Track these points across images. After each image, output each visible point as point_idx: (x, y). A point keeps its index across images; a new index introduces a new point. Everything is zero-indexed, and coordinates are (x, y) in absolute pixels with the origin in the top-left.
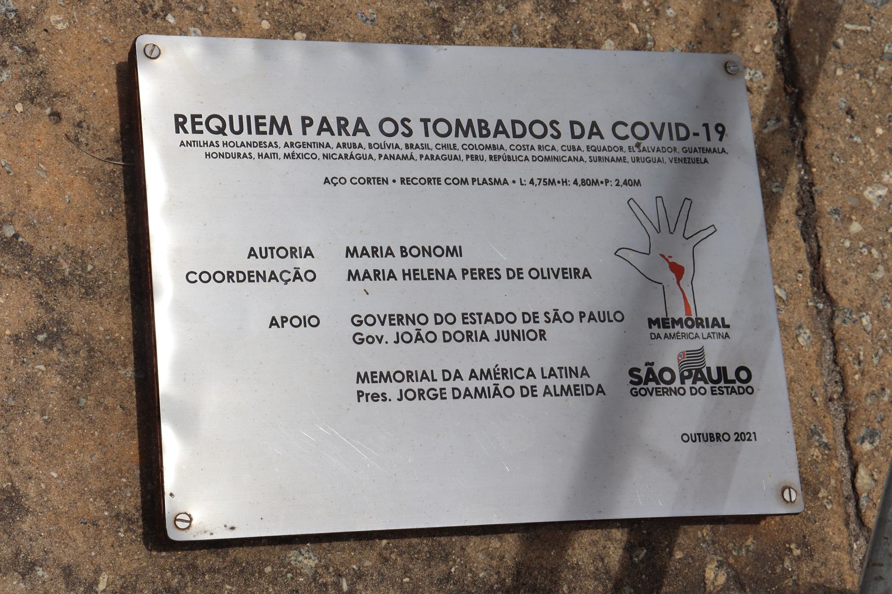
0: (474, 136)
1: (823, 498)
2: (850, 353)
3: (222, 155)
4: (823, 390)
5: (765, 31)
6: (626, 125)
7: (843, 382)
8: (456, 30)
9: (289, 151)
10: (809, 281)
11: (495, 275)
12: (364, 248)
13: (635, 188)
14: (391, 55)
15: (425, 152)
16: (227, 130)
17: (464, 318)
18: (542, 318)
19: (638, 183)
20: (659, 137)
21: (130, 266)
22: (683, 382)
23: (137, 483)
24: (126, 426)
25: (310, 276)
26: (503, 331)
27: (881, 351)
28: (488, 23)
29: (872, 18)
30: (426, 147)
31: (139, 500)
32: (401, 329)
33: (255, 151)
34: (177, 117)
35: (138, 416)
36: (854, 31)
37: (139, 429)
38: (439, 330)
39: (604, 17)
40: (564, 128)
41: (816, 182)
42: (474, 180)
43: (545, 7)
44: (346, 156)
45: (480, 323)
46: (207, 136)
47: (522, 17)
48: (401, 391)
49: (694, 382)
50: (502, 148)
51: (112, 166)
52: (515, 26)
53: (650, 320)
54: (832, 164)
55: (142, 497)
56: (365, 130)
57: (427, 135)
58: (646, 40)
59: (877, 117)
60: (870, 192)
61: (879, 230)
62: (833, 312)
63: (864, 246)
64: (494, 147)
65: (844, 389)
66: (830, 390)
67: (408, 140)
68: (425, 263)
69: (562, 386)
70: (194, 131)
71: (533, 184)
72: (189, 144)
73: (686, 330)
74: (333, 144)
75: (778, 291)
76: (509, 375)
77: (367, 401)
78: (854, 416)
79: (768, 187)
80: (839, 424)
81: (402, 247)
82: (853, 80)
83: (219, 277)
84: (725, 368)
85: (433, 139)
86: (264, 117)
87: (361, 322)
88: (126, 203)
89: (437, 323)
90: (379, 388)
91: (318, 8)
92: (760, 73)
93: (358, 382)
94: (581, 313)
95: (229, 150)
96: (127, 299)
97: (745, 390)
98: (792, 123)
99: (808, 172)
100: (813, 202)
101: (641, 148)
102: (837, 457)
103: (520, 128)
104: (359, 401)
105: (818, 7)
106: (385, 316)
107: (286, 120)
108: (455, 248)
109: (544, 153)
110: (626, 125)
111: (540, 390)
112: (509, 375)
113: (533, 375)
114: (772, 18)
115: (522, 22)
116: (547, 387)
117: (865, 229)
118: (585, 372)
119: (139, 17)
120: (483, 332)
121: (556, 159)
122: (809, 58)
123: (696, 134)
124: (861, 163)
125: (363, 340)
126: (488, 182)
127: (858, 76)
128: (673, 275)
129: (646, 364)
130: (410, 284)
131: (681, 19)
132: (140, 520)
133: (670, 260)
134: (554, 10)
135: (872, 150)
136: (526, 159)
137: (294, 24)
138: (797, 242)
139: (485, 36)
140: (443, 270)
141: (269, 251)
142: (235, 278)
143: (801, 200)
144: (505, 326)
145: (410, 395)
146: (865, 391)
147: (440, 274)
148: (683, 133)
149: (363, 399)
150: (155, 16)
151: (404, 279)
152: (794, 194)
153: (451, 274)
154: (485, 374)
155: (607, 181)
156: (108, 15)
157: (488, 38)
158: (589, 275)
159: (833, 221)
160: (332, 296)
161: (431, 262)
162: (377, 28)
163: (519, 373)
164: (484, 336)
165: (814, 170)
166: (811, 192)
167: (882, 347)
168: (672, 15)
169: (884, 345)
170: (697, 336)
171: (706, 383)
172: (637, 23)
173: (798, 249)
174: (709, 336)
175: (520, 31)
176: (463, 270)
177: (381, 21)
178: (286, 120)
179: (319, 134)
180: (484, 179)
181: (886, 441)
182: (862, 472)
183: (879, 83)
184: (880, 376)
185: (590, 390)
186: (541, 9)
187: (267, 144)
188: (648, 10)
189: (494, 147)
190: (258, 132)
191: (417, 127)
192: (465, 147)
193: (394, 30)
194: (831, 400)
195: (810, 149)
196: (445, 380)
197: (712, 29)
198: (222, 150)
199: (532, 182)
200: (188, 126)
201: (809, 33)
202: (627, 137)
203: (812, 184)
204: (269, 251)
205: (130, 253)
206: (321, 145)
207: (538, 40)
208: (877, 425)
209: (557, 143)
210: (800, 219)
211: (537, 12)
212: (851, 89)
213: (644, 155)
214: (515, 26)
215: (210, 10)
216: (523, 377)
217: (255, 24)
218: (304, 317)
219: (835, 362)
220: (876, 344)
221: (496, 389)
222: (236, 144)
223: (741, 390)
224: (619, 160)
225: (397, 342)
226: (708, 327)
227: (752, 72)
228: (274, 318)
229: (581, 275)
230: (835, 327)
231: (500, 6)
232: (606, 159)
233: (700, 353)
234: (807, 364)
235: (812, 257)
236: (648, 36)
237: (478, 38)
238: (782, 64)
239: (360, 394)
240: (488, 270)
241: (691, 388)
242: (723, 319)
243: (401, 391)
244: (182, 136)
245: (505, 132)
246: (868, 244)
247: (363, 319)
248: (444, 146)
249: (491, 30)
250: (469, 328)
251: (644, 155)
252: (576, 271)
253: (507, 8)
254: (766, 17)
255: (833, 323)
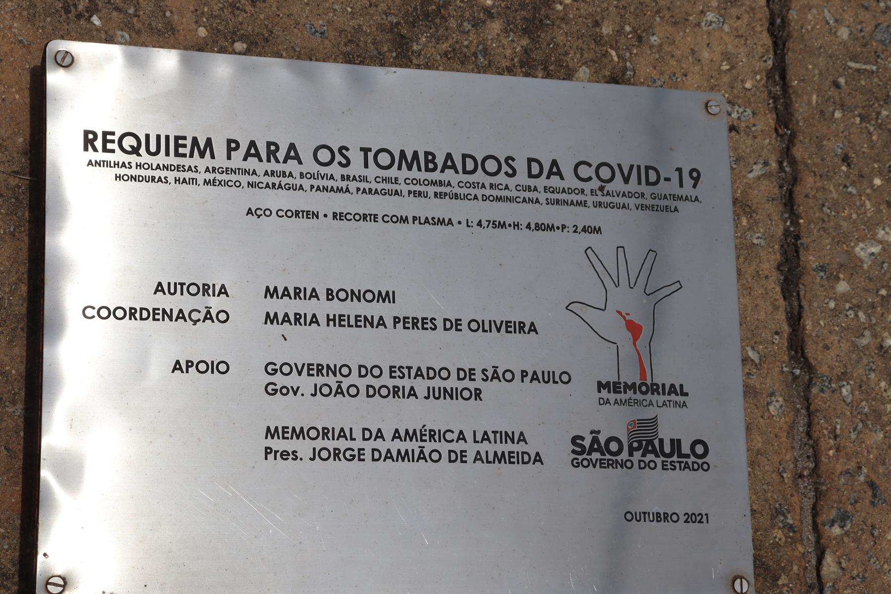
0: (419, 169)
1: (783, 585)
2: (826, 425)
3: (133, 178)
4: (792, 465)
5: (759, 65)
6: (590, 165)
7: (816, 457)
8: (415, 47)
9: (210, 176)
10: (786, 344)
11: (430, 325)
12: (286, 289)
13: (594, 236)
14: (334, 75)
15: (362, 185)
16: (142, 150)
17: (391, 372)
18: (479, 376)
19: (598, 230)
20: (626, 180)
21: (29, 292)
22: (631, 454)
23: (17, 534)
24: (9, 470)
25: (223, 317)
26: (434, 388)
27: (860, 425)
28: (450, 41)
29: (878, 56)
30: (364, 179)
31: (17, 554)
32: (320, 380)
33: (171, 175)
34: (86, 133)
35: (24, 459)
36: (858, 70)
37: (23, 473)
38: (362, 383)
39: (580, 41)
40: (521, 166)
41: (802, 234)
42: (415, 218)
43: (516, 27)
44: (274, 185)
45: (410, 378)
46: (119, 156)
47: (490, 37)
48: (314, 449)
49: (644, 455)
50: (449, 184)
51: (17, 181)
52: (481, 47)
53: (599, 383)
54: (822, 216)
55: (21, 550)
56: (297, 158)
57: (366, 166)
58: (625, 69)
59: (876, 166)
60: (862, 249)
61: (868, 291)
62: (811, 380)
63: (850, 308)
64: (441, 183)
65: (816, 465)
66: (800, 465)
67: (345, 171)
68: (353, 308)
69: (496, 453)
70: (105, 150)
71: (481, 226)
72: (98, 163)
73: (639, 396)
74: (260, 172)
75: (751, 354)
76: (436, 437)
77: (275, 459)
78: (824, 496)
79: (748, 237)
80: (808, 503)
81: (328, 290)
82: (852, 123)
83: (120, 313)
84: (679, 441)
85: (373, 171)
86: (184, 138)
87: (276, 371)
88: (29, 221)
89: (360, 376)
90: (289, 445)
91: (262, 16)
92: (749, 111)
93: (266, 438)
94: (523, 371)
95: (142, 172)
96: (22, 329)
97: (701, 466)
98: (781, 168)
99: (795, 223)
100: (798, 257)
101: (605, 192)
102: (802, 540)
103: (471, 164)
104: (266, 458)
105: (820, 42)
106: (304, 365)
107: (209, 142)
108: (387, 293)
109: (496, 193)
110: (590, 165)
111: (470, 456)
112: (436, 437)
113: (464, 439)
114: (767, 51)
115: (489, 43)
116: (478, 453)
117: (853, 289)
118: (522, 438)
119: (61, 16)
120: (412, 388)
121: (509, 199)
122: (805, 97)
123: (667, 179)
124: (854, 216)
125: (276, 391)
126: (431, 222)
127: (858, 120)
128: (629, 335)
129: (592, 432)
130: (335, 331)
131: (666, 48)
132: (16, 576)
133: (628, 318)
134: (525, 31)
135: (867, 202)
136: (476, 197)
137: (235, 33)
138: (776, 300)
139: (446, 56)
140: (372, 317)
141: (179, 287)
142: (137, 315)
143: (784, 253)
144: (437, 383)
145: (324, 454)
146: (839, 468)
147: (369, 322)
148: (653, 177)
149: (271, 457)
150: (79, 16)
151: (328, 325)
152: (776, 247)
153: (381, 322)
154: (410, 435)
155: (564, 227)
156: (25, 13)
157: (449, 59)
158: (535, 330)
159: (819, 278)
160: (244, 339)
161: (359, 307)
162: (326, 42)
163: (449, 436)
164: (413, 393)
165: (801, 221)
166: (796, 246)
167: (862, 421)
168: (656, 43)
169: (864, 418)
170: (651, 403)
171: (657, 456)
172: (617, 50)
173: (776, 308)
174: (664, 404)
175: (486, 52)
176: (395, 318)
177: (332, 34)
178: (209, 142)
179: (245, 159)
180: (427, 218)
181: (858, 525)
182: (829, 559)
183: (881, 129)
184: (857, 453)
185: (526, 458)
186: (511, 30)
187: (186, 168)
188: (630, 36)
189: (441, 183)
190: (177, 154)
191: (356, 157)
192: (407, 181)
193: (346, 45)
194: (801, 476)
195: (799, 198)
196: (364, 439)
197: (699, 60)
198: (134, 172)
199: (479, 224)
200: (99, 144)
201: (807, 69)
202: (590, 179)
203: (797, 237)
204: (179, 287)
205: (29, 278)
206: (246, 172)
207: (505, 63)
208: (850, 507)
209: (512, 182)
210: (782, 274)
211: (506, 32)
212: (850, 134)
213: (608, 199)
214: (481, 47)
215: (141, 13)
216: (453, 440)
217: (190, 31)
218: (212, 362)
219: (809, 434)
220: (856, 417)
221: (422, 452)
222: (150, 167)
223: (696, 466)
224: (579, 204)
225: (314, 395)
226: (664, 394)
227: (741, 110)
228: (178, 362)
229: (526, 329)
230: (812, 396)
231: (465, 24)
232: (565, 202)
233: (653, 422)
234: (776, 436)
235: (791, 317)
236: (628, 64)
237: (439, 58)
238: (774, 102)
239: (268, 451)
240: (423, 319)
241: (640, 461)
242: (681, 386)
243: (314, 449)
244: (91, 155)
245: (454, 167)
246: (855, 306)
247: (278, 367)
248: (385, 180)
249: (454, 50)
250: (397, 381)
251: (608, 199)
252: (522, 325)
253: (473, 26)
254: (761, 50)
255: (810, 391)
